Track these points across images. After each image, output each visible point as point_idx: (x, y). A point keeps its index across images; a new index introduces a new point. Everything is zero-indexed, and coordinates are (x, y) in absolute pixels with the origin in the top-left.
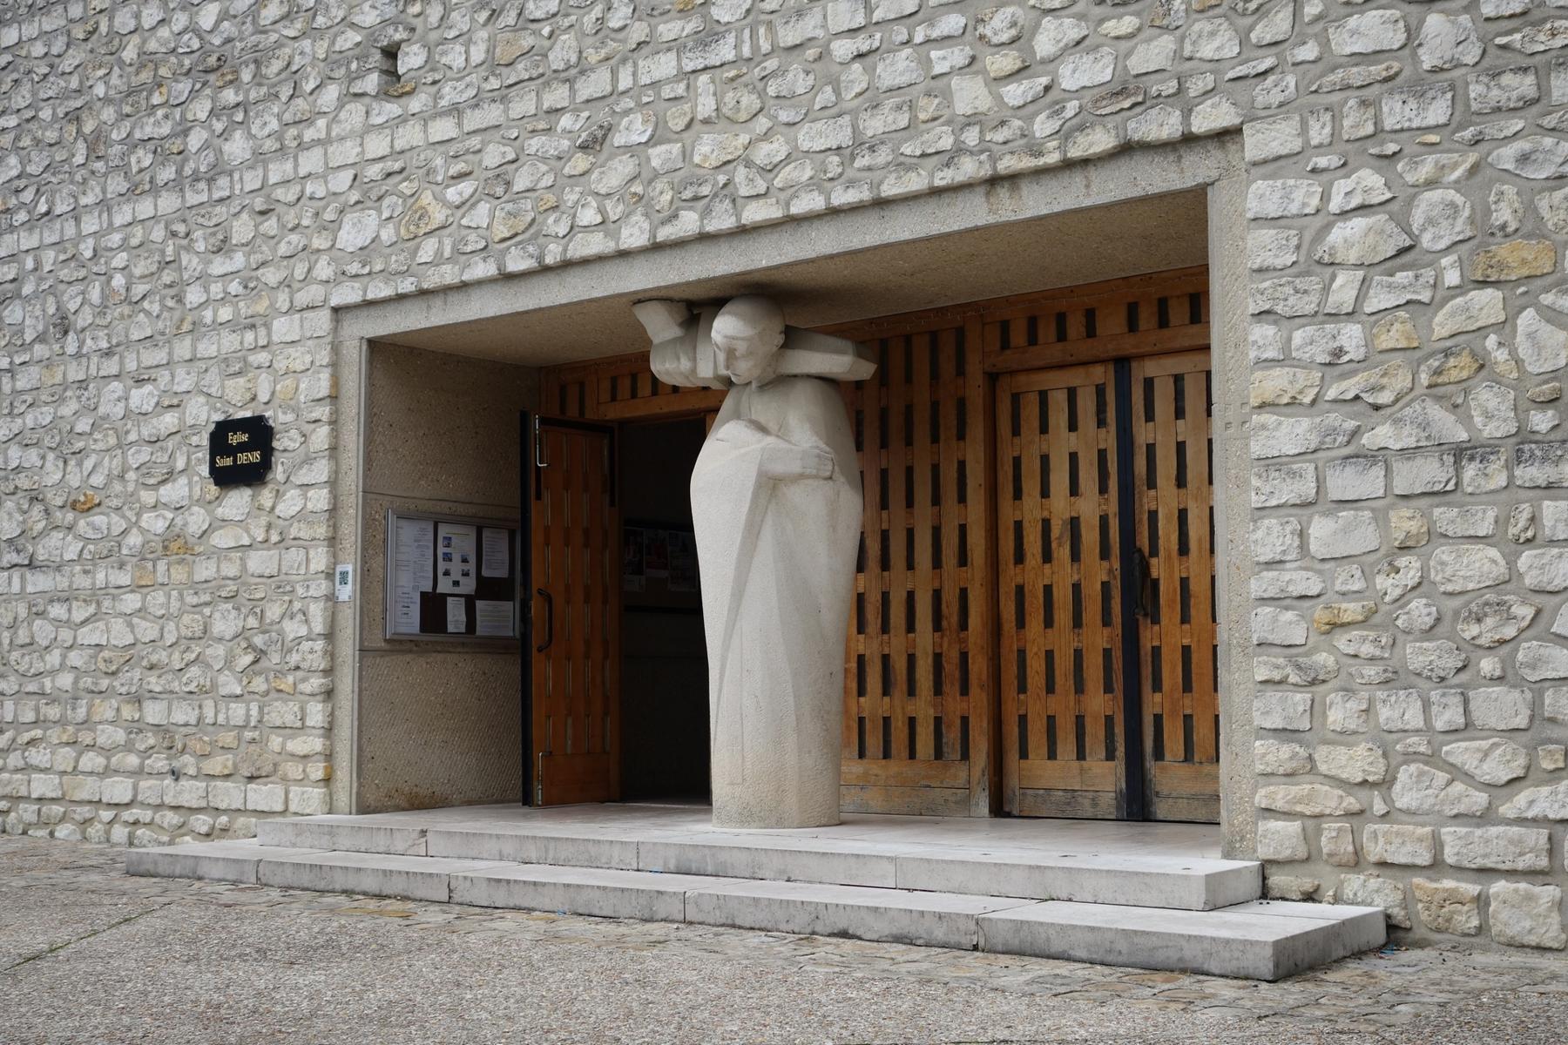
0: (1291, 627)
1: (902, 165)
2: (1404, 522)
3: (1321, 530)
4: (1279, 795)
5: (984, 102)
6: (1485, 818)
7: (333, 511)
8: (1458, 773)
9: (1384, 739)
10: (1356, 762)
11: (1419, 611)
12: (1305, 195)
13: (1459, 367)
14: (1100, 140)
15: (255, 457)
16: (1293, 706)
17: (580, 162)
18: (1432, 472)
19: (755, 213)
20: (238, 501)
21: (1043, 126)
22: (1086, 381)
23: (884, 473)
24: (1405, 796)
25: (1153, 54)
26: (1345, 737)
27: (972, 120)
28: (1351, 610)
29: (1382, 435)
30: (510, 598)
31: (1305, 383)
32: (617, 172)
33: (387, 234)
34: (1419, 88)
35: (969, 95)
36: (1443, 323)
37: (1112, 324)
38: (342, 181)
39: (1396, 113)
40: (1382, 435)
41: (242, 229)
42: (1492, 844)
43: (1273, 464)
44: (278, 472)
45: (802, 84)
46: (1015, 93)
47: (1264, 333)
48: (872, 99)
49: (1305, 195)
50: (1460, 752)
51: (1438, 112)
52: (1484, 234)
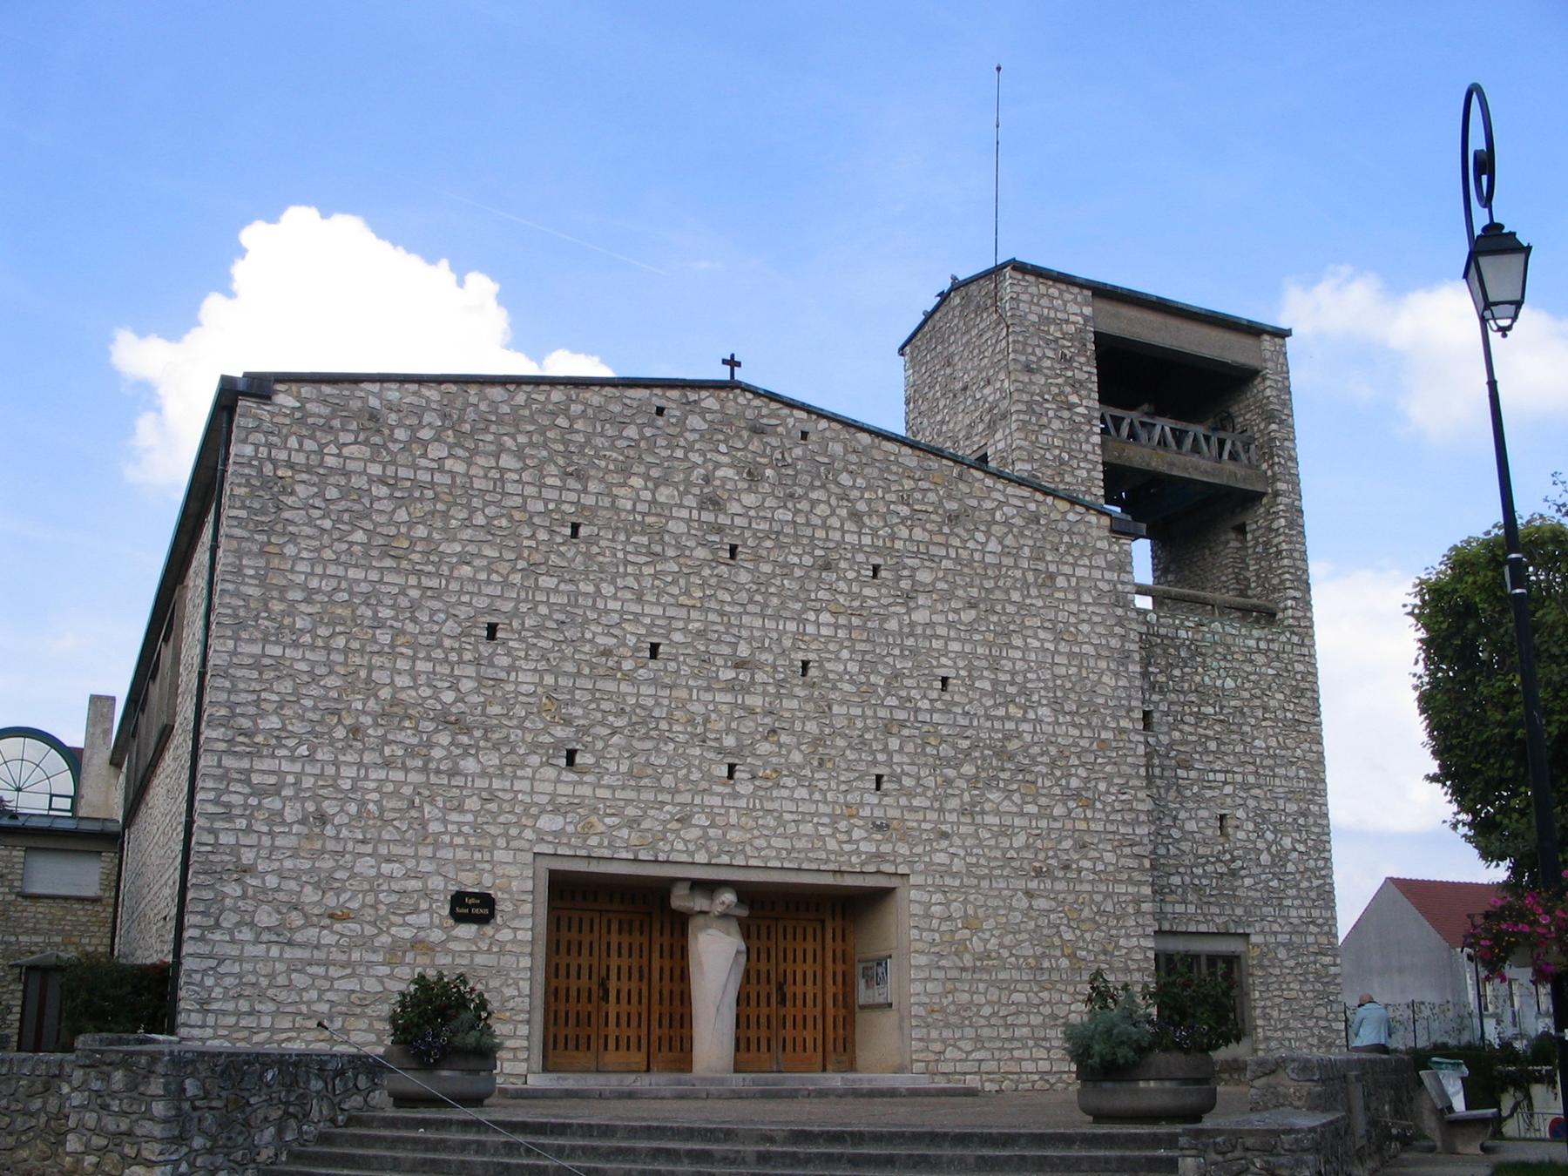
1: (810, 860)
2: (949, 986)
3: (929, 986)
4: (921, 1056)
5: (836, 848)
6: (966, 1060)
7: (533, 942)
8: (960, 1049)
9: (944, 1041)
10: (937, 1047)
11: (952, 1008)
12: (926, 897)
13: (961, 948)
14: (872, 868)
15: (486, 911)
16: (922, 1033)
17: (675, 825)
19: (752, 862)
20: (467, 930)
21: (854, 859)
23: (558, 920)
24: (948, 1055)
25: (886, 848)
26: (934, 1041)
27: (833, 852)
28: (936, 1007)
29: (943, 963)
30: (1467, 1108)
31: (926, 947)
34: (954, 875)
35: (832, 844)
36: (957, 937)
39: (948, 881)
40: (943, 963)
42: (968, 1066)
43: (918, 967)
45: (772, 823)
46: (847, 847)
47: (914, 932)
48: (798, 835)
50: (961, 1044)
51: (957, 883)
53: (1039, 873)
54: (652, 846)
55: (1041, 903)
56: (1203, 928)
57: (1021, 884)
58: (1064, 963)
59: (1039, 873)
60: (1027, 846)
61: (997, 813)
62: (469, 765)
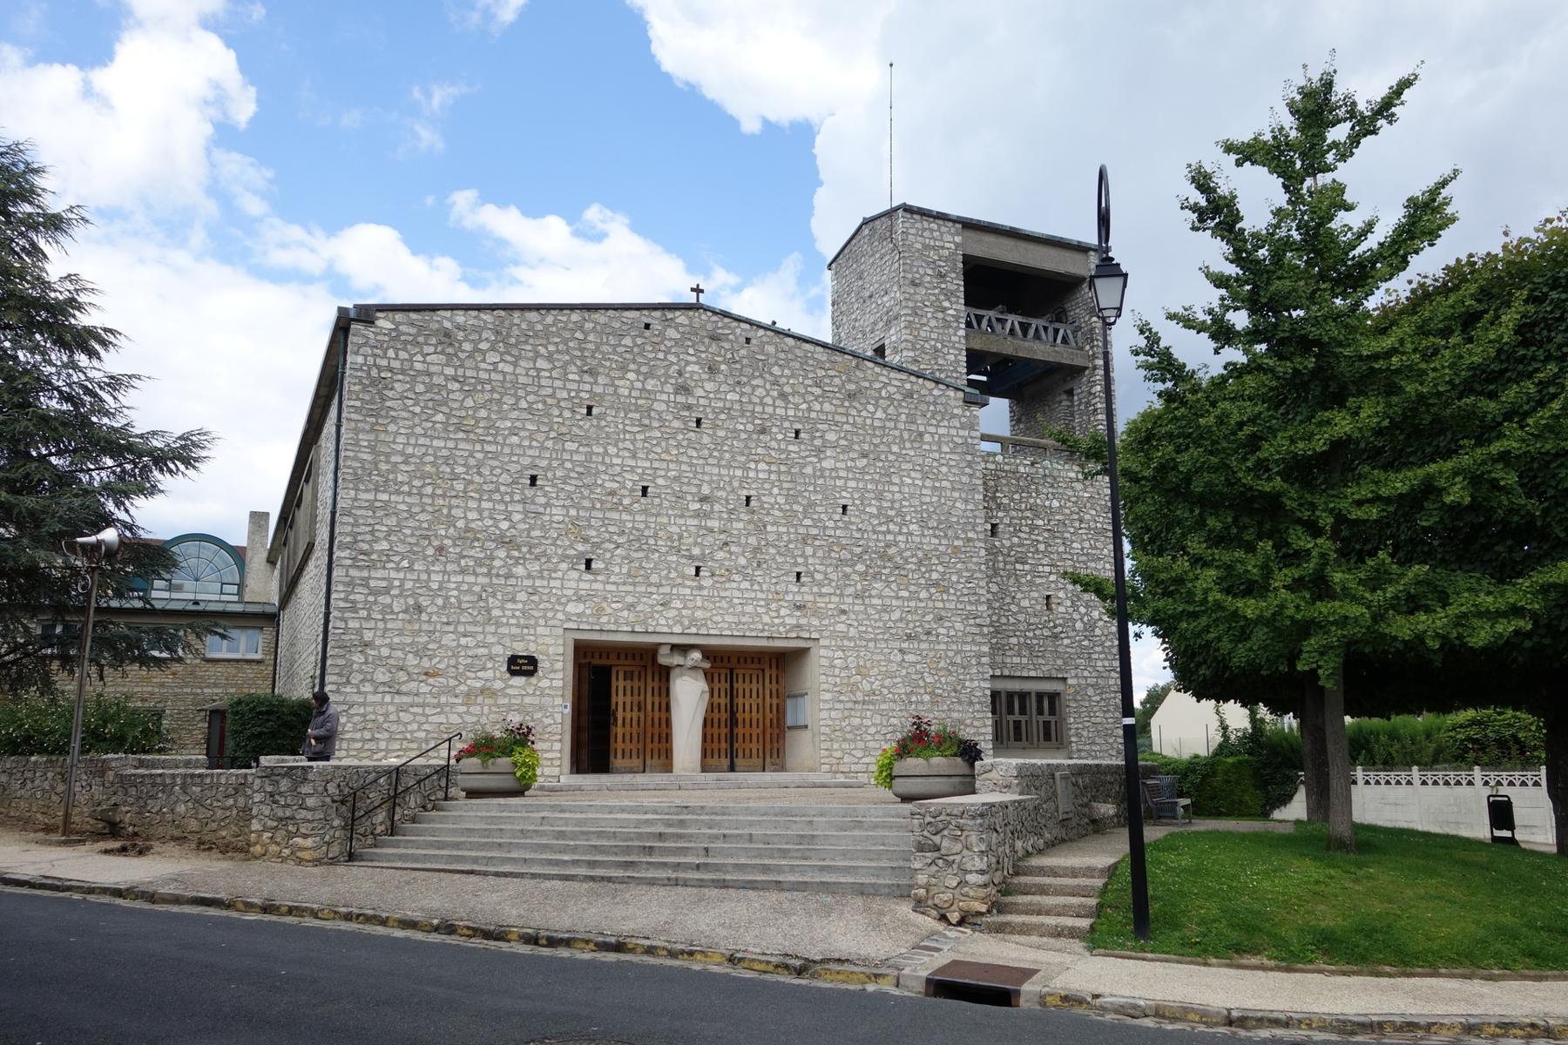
0: (827, 731)
12: (831, 654)
18: (850, 705)
20: (519, 681)
22: (723, 672)
32: (672, 613)
33: (588, 612)
34: (850, 639)
35: (766, 619)
37: (734, 660)
38: (570, 592)
39: (846, 643)
41: (522, 596)
43: (825, 701)
44: (540, 673)
49: (831, 654)
52: (859, 666)
53: (909, 637)
54: (644, 622)
55: (910, 658)
56: (1033, 674)
57: (897, 644)
58: (927, 698)
59: (909, 637)
60: (901, 620)
61: (880, 597)
62: (519, 571)
